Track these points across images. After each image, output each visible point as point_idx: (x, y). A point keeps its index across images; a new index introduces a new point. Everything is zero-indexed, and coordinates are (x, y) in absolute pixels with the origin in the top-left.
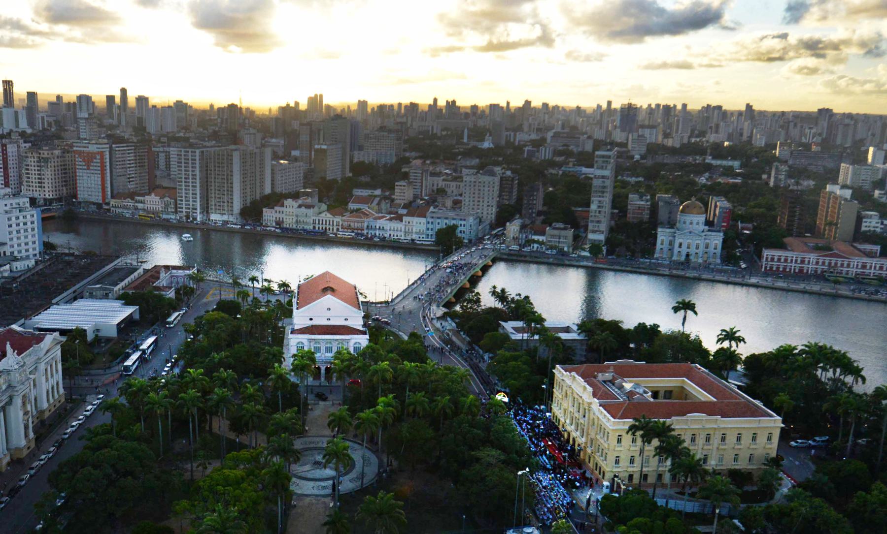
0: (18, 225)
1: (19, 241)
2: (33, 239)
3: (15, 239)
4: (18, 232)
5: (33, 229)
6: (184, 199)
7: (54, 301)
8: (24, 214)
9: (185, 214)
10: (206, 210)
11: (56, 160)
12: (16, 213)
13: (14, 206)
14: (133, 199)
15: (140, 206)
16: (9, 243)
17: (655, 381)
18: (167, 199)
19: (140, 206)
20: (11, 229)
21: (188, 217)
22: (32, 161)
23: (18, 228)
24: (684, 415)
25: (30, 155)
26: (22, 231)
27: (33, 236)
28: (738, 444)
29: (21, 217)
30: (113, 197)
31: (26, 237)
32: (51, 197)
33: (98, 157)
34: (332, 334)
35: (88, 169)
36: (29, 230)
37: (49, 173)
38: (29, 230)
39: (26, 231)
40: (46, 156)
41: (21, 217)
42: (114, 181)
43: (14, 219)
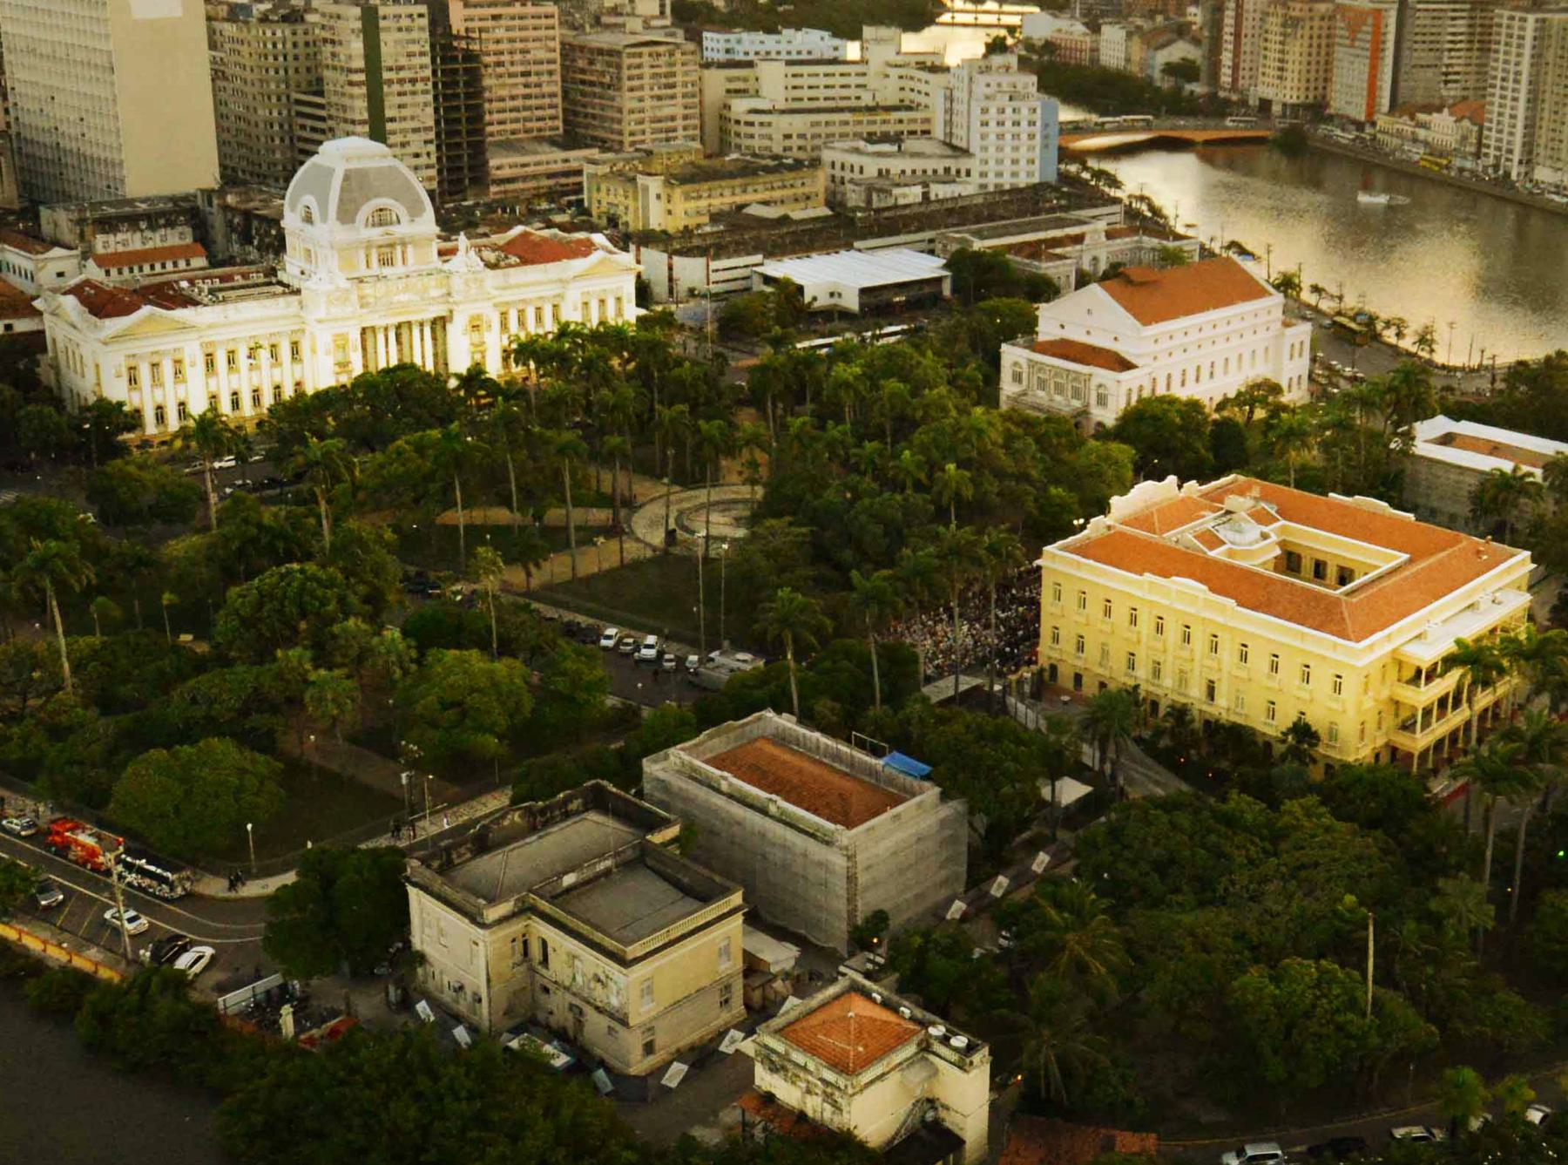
0: (1000, 124)
1: (1000, 155)
2: (1030, 155)
3: (992, 150)
4: (1000, 136)
5: (1031, 137)
6: (1494, 125)
7: (857, 244)
8: (1015, 104)
9: (1491, 161)
10: (1528, 161)
11: (1316, 23)
12: (1002, 100)
13: (1005, 88)
14: (1412, 118)
15: (1422, 133)
16: (979, 155)
17: (1339, 544)
18: (1466, 123)
19: (1422, 133)
20: (985, 129)
21: (1496, 167)
22: (1274, 24)
23: (1000, 130)
24: (1166, 575)
25: (1271, 10)
26: (1008, 137)
27: (1031, 149)
28: (1269, 677)
29: (1009, 111)
30: (1394, 106)
31: (1016, 149)
32: (1294, 100)
33: (1370, 21)
34: (1074, 360)
35: (1352, 46)
36: (1024, 137)
37: (1297, 49)
38: (1024, 137)
39: (1016, 136)
40: (1296, 13)
41: (1009, 111)
42: (1402, 76)
43: (993, 111)
